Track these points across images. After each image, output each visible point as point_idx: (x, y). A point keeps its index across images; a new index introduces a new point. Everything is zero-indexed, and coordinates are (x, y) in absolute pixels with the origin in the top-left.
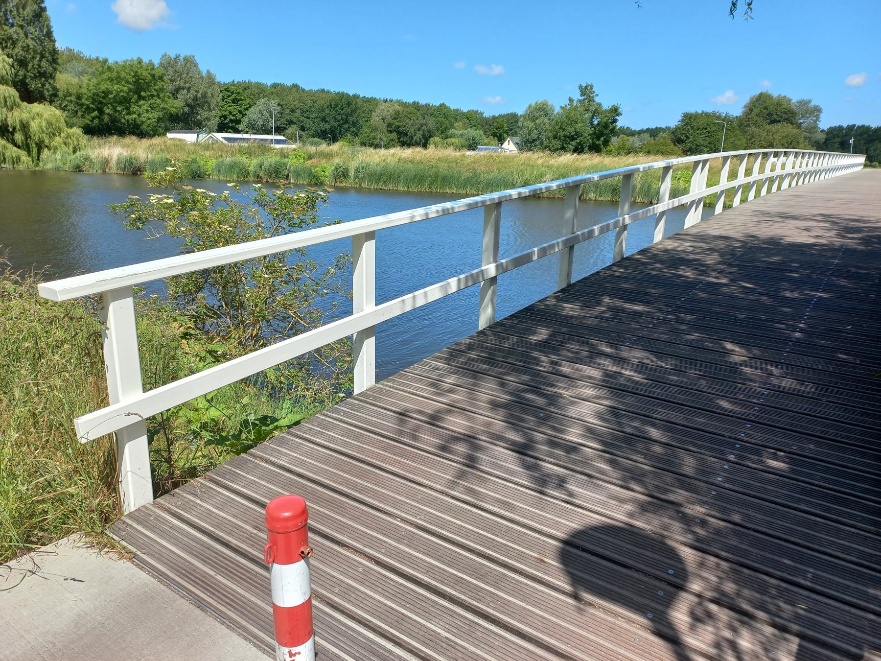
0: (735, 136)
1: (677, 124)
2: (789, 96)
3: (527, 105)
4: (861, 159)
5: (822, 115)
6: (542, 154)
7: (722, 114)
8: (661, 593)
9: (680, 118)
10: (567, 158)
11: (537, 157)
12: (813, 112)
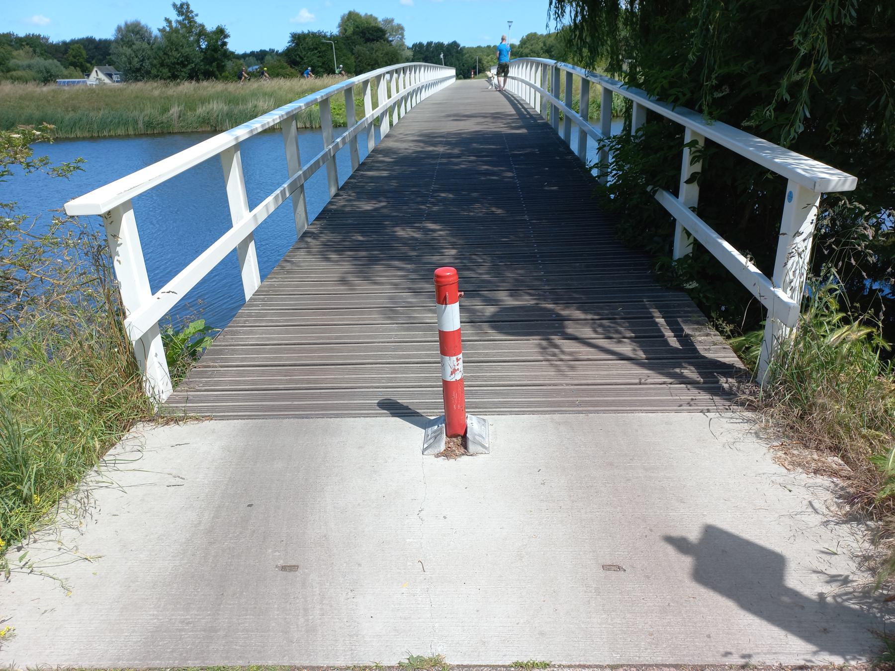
0: (344, 56)
1: (288, 45)
2: (375, 15)
3: (115, 27)
4: (452, 72)
5: (405, 33)
6: (155, 84)
7: (327, 34)
8: (557, 325)
9: (289, 39)
10: (187, 87)
11: (150, 88)
12: (397, 30)
